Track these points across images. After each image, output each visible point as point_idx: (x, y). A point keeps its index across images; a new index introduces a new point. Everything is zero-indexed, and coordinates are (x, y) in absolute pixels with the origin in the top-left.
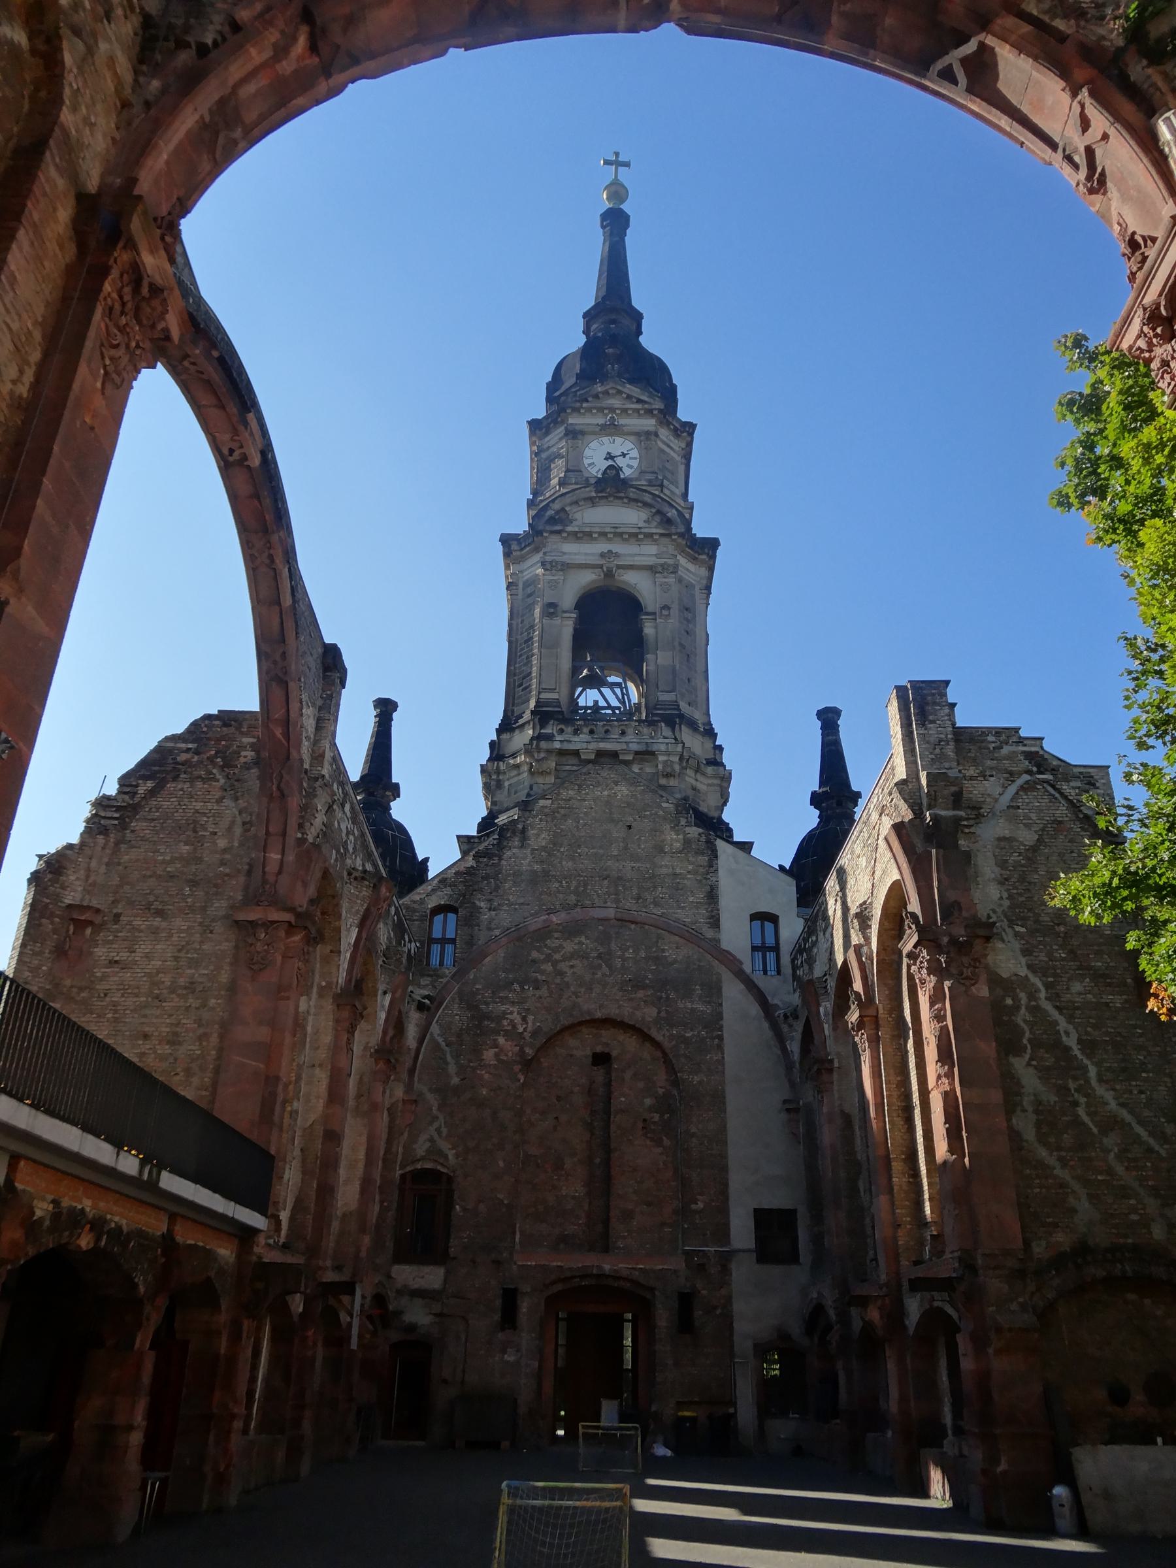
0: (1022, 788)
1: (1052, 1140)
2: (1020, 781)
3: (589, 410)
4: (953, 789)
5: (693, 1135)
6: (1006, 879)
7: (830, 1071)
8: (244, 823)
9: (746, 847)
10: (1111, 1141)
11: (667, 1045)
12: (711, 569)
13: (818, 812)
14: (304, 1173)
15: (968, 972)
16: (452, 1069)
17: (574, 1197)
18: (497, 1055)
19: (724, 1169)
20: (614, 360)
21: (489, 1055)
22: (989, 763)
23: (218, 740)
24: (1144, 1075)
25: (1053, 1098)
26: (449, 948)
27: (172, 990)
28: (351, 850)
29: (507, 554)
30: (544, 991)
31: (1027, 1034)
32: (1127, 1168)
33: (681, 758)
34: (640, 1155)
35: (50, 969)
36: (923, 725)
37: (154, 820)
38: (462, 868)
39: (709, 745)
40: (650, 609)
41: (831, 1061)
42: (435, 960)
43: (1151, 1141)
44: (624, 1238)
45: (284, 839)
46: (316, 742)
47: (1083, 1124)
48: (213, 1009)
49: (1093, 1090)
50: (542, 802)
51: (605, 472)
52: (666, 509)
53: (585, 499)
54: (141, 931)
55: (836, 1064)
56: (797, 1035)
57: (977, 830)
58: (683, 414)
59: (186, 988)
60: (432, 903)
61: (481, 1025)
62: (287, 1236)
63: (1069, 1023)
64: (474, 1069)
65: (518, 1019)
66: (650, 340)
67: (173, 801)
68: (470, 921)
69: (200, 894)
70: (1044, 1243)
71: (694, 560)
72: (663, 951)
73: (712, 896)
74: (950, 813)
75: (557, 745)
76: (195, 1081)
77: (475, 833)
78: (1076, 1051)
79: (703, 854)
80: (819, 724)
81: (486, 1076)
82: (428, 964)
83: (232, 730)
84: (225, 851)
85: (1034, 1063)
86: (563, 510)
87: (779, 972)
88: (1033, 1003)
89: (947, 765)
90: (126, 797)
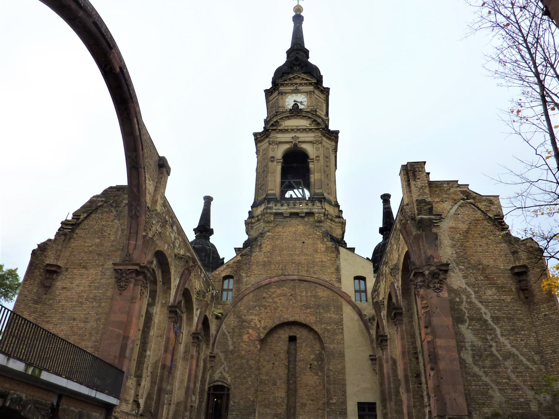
0: (460, 206)
1: (480, 363)
2: (459, 204)
3: (287, 84)
4: (429, 206)
5: (331, 370)
6: (454, 245)
7: (386, 340)
8: (122, 230)
9: (352, 250)
10: (508, 363)
11: (320, 332)
12: (337, 142)
13: (382, 236)
14: (152, 383)
15: (438, 285)
16: (230, 343)
17: (281, 397)
18: (249, 337)
19: (344, 385)
20: (298, 68)
21: (245, 337)
22: (445, 196)
23: (114, 196)
24: (523, 332)
25: (480, 343)
26: (230, 293)
27: (87, 300)
28: (177, 245)
29: (256, 140)
30: (268, 310)
31: (467, 315)
32: (517, 376)
33: (324, 214)
34: (309, 379)
35: (37, 291)
36: (414, 180)
37: (85, 229)
38: (235, 260)
39: (337, 210)
40: (311, 157)
41: (387, 336)
42: (224, 298)
43: (528, 363)
44: (302, 415)
45: (137, 235)
46: (154, 196)
47: (495, 355)
48: (103, 307)
49: (499, 339)
50: (268, 234)
51: (293, 106)
52: (317, 119)
53: (286, 117)
54: (76, 275)
55: (389, 337)
56: (375, 327)
57: (441, 224)
58: (325, 85)
59: (93, 298)
60: (223, 274)
61: (243, 324)
62: (143, 410)
63: (486, 309)
64: (239, 343)
65: (258, 323)
66: (312, 60)
67: (94, 222)
68: (238, 282)
69: (102, 259)
70: (478, 413)
71: (329, 139)
72: (318, 292)
73: (338, 270)
74: (428, 217)
75: (274, 211)
76: (93, 338)
77: (242, 247)
78: (490, 321)
79: (334, 252)
80: (382, 201)
81: (244, 346)
82: (221, 299)
83: (120, 192)
84: (113, 241)
85: (471, 327)
86: (277, 121)
87: (367, 301)
88: (469, 300)
89: (425, 196)
90: (75, 220)
